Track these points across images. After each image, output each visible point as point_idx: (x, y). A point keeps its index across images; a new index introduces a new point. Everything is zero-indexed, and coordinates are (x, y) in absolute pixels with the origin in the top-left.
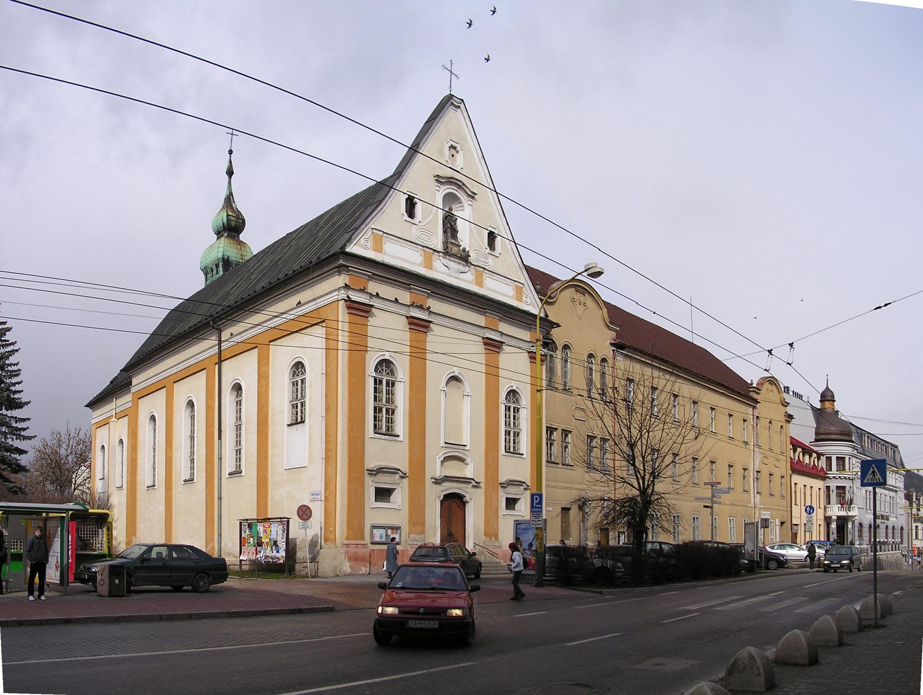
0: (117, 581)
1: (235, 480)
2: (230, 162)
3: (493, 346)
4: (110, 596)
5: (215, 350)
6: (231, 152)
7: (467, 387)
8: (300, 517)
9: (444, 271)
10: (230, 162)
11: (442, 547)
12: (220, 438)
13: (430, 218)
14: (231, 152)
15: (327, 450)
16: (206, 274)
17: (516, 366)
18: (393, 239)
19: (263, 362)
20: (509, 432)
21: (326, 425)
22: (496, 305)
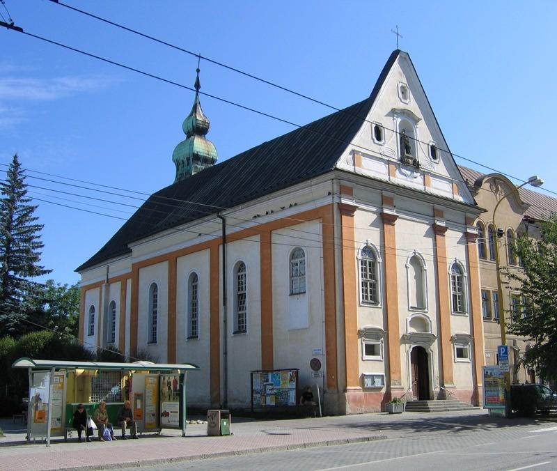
0: (225, 423)
1: (240, 338)
2: (198, 78)
3: (437, 231)
4: (209, 435)
5: (220, 234)
6: (198, 71)
7: (298, 243)
8: (313, 369)
9: (402, 178)
10: (198, 78)
11: (297, 405)
12: (225, 304)
13: (391, 146)
14: (198, 71)
15: (327, 316)
16: (178, 165)
17: (454, 247)
18: (366, 156)
19: (266, 246)
20: (366, 284)
21: (326, 297)
22: (412, 193)
